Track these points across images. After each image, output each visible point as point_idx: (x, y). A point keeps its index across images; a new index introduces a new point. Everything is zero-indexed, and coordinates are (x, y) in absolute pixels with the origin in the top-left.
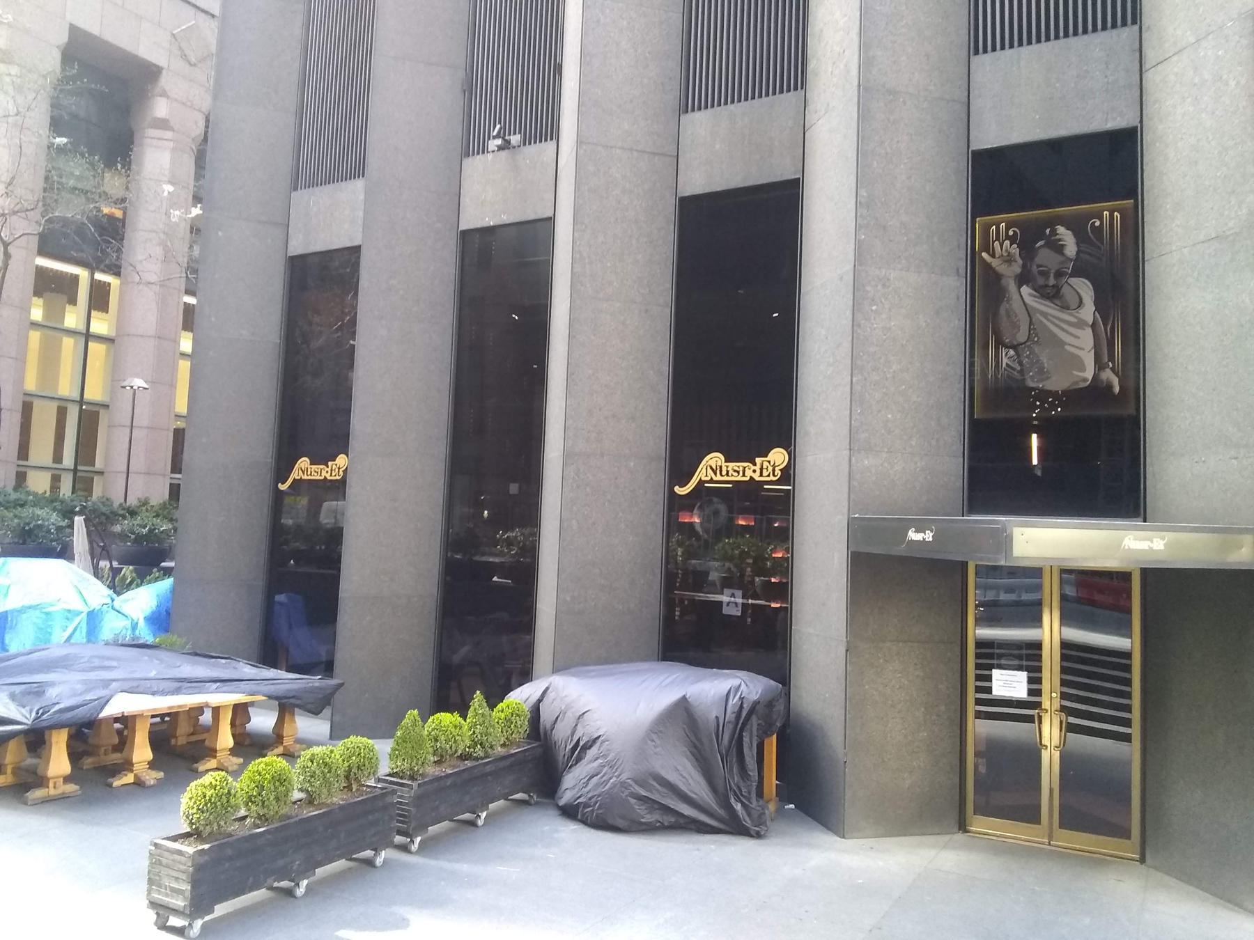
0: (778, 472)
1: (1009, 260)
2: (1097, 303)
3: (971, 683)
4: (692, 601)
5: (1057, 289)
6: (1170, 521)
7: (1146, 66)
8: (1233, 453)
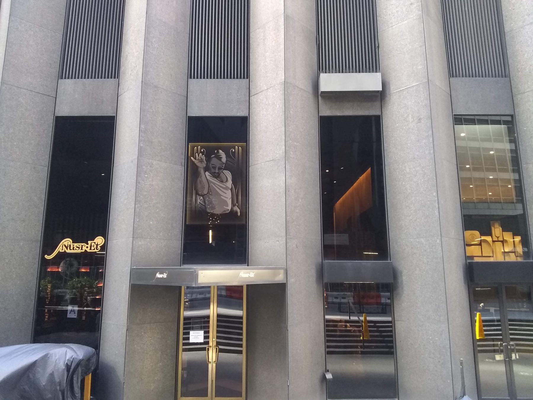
0: (99, 248)
1: (201, 161)
2: (233, 181)
3: (181, 336)
4: (55, 311)
5: (219, 174)
6: (257, 265)
7: (251, 94)
8: (277, 239)
